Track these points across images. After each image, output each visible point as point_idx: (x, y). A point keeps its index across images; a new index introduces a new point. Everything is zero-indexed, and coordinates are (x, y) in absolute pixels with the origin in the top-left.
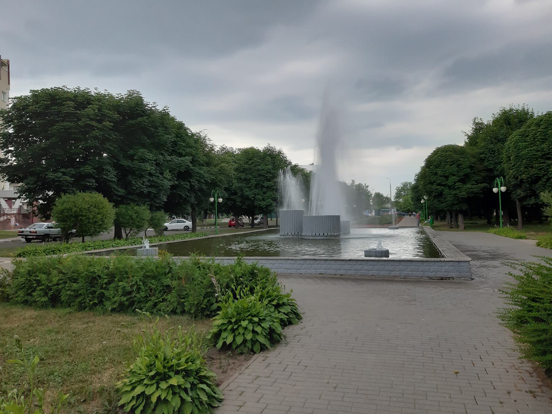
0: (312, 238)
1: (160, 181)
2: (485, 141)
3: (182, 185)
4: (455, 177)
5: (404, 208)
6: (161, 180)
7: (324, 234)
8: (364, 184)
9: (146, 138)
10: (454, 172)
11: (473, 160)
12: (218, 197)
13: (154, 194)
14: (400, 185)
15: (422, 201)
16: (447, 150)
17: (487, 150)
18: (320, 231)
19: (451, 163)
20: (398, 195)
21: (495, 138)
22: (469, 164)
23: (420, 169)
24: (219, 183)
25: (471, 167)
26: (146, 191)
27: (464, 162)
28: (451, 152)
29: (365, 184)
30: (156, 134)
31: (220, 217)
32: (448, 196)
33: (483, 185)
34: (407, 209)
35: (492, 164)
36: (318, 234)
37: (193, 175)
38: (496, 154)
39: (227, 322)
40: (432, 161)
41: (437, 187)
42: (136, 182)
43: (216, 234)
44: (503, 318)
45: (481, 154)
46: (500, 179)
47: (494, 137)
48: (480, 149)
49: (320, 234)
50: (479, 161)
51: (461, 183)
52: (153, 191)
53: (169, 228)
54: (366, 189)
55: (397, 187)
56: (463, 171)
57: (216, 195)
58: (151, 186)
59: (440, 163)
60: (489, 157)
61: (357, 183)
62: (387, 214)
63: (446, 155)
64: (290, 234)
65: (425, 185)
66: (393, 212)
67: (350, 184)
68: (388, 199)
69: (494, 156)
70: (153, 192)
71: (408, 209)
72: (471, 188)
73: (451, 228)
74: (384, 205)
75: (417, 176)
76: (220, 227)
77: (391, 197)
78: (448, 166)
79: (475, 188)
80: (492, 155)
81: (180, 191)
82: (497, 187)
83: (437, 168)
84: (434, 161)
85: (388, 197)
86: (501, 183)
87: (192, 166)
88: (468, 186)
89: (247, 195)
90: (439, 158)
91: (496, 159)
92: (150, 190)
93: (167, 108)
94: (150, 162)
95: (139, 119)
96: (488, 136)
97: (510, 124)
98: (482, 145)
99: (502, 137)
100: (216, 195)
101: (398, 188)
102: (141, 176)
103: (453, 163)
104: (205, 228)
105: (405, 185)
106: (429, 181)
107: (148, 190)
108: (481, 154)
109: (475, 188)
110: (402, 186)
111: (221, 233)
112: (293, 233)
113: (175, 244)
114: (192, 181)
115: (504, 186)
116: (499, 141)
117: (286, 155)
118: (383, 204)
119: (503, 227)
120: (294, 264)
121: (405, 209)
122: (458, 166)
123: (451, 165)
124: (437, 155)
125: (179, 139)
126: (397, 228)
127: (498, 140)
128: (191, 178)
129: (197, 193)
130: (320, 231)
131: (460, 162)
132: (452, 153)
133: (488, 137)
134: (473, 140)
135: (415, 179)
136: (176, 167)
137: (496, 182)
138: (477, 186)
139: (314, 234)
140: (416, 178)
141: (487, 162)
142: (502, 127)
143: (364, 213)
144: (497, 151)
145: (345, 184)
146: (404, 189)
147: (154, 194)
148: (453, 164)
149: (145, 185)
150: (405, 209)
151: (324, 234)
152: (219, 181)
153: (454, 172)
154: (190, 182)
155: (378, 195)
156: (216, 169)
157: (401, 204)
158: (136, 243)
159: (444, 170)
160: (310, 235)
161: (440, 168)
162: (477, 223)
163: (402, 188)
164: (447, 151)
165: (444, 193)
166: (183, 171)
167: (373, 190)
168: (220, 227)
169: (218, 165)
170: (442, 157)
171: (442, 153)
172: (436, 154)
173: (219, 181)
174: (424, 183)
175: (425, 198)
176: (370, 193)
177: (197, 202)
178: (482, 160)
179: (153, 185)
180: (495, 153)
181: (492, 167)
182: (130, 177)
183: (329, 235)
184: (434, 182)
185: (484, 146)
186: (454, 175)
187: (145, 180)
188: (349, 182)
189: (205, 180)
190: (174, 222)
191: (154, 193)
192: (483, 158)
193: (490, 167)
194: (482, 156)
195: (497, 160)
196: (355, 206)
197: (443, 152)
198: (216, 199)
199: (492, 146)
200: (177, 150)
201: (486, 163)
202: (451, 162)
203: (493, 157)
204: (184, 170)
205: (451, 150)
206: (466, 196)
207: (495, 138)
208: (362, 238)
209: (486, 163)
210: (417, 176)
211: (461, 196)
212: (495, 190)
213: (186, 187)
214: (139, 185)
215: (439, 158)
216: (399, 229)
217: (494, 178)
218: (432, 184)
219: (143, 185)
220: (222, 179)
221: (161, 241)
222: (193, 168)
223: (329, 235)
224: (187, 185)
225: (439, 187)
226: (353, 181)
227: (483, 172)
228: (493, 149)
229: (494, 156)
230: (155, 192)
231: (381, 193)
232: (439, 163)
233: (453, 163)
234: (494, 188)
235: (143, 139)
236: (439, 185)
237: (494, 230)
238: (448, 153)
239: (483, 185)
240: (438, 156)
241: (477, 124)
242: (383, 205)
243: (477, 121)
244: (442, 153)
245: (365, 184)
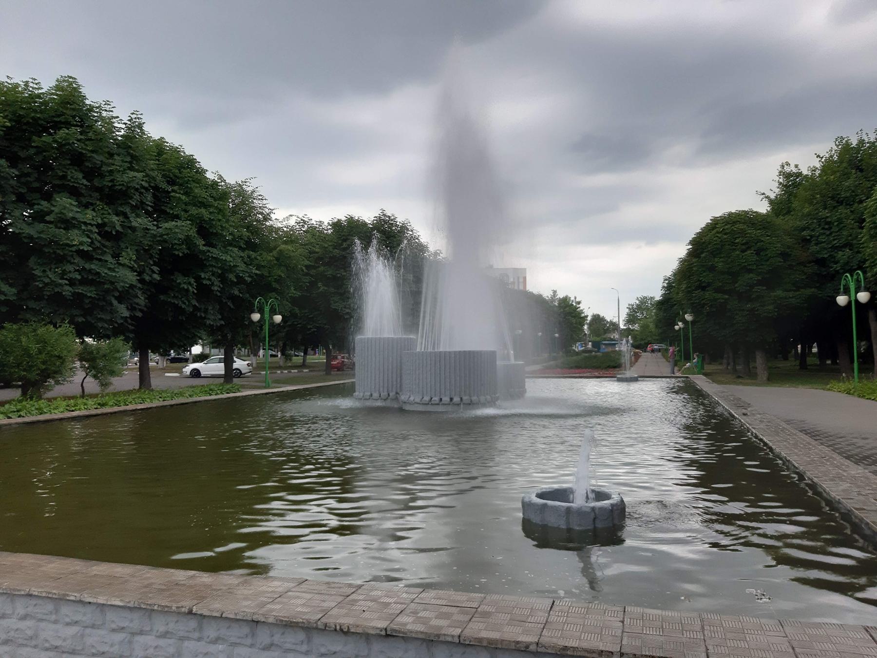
0: (421, 408)
1: (106, 271)
2: (811, 203)
3: (180, 284)
4: (751, 275)
5: (642, 339)
6: (109, 269)
7: (451, 399)
8: (572, 299)
9: (80, 175)
10: (750, 265)
11: (788, 240)
12: (273, 312)
13: (90, 300)
14: (635, 301)
15: (677, 327)
16: (735, 220)
17: (815, 221)
18: (443, 391)
19: (744, 247)
20: (631, 319)
21: (833, 198)
22: (782, 250)
23: (678, 262)
24: (275, 285)
25: (784, 255)
26: (67, 291)
27: (770, 244)
28: (744, 223)
29: (575, 298)
30: (104, 168)
31: (311, 352)
32: (737, 314)
33: (809, 291)
35: (825, 249)
36: (436, 399)
37: (206, 264)
38: (835, 229)
40: (704, 243)
41: (714, 295)
42: (44, 271)
43: (265, 388)
45: (804, 229)
46: (855, 277)
47: (830, 195)
48: (800, 221)
49: (441, 400)
50: (799, 244)
51: (765, 288)
52: (90, 292)
53: (203, 373)
54: (576, 306)
55: (629, 305)
56: (768, 263)
57: (267, 309)
58: (84, 282)
59: (722, 246)
60: (819, 236)
61: (561, 295)
62: (613, 350)
63: (732, 230)
64: (376, 395)
65: (689, 292)
66: (624, 347)
67: (550, 296)
68: (615, 326)
69: (831, 234)
70: (89, 295)
72: (786, 298)
73: (739, 377)
74: (608, 335)
75: (667, 282)
76: (310, 371)
77: (619, 321)
78: (738, 252)
79: (793, 297)
80: (825, 231)
81: (175, 297)
82: (847, 292)
83: (714, 257)
84: (709, 244)
85: (614, 321)
87: (204, 245)
88: (779, 293)
89: (335, 309)
90: (719, 235)
91: (834, 240)
92: (80, 290)
93: (139, 116)
94: (83, 228)
95: (63, 132)
96: (817, 194)
97: (861, 171)
98: (806, 211)
99: (848, 195)
100: (267, 309)
101: (631, 307)
102: (61, 260)
103: (747, 246)
104: (279, 372)
105: (643, 301)
106: (698, 283)
107: (72, 291)
108: (804, 229)
109: (793, 297)
110: (637, 302)
111: (279, 385)
112: (384, 394)
113: (175, 407)
114: (203, 277)
115: (866, 289)
116: (840, 203)
117: (418, 234)
118: (605, 333)
119: (860, 378)
120: (93, 626)
122: (758, 252)
123: (743, 251)
124: (715, 231)
125: (176, 188)
126: (635, 380)
127: (838, 202)
128: (203, 271)
129: (226, 303)
130: (443, 391)
131: (762, 243)
132: (745, 226)
133: (818, 196)
134: (781, 206)
135: (664, 287)
136: (153, 241)
137: (843, 282)
138: (798, 293)
139: (427, 398)
140: (666, 285)
141: (816, 244)
142: (846, 175)
143: (574, 348)
144: (836, 224)
145: (540, 297)
146: (641, 307)
147: (90, 300)
148: (749, 248)
149: (66, 279)
151: (451, 399)
152: (276, 281)
153: (750, 265)
154: (198, 279)
155: (597, 319)
156: (269, 257)
157: (637, 333)
158: (22, 413)
159: (730, 260)
160: (418, 400)
161: (721, 258)
162: (779, 368)
163: (637, 305)
164: (734, 222)
165: (728, 307)
166: (181, 255)
167: (589, 309)
168: (310, 371)
169: (275, 248)
170: (725, 234)
171: (726, 227)
172: (713, 230)
173: (276, 281)
174: (686, 288)
175: (688, 317)
176: (583, 313)
177: (224, 323)
178: (806, 241)
179: (90, 279)
180: (831, 228)
181: (826, 256)
182: (32, 262)
183: (464, 401)
184: (709, 285)
185: (809, 214)
186: (750, 271)
187: (69, 268)
188: (547, 294)
189: (237, 277)
190: (211, 361)
191: (91, 297)
192: (809, 238)
193: (821, 256)
194: (804, 233)
195: (835, 242)
196: (557, 335)
197: (726, 225)
198: (267, 316)
199: (825, 213)
200: (168, 210)
201: (814, 248)
202: (743, 244)
203: (827, 235)
204: (183, 253)
205: (743, 221)
206: (776, 314)
207: (833, 198)
209: (814, 248)
210: (667, 282)
211: (766, 314)
212: (842, 300)
213: (186, 287)
214: (50, 278)
215: (719, 235)
216: (639, 383)
217: (835, 277)
218: (704, 288)
219: (62, 278)
220: (280, 276)
221: (102, 405)
222: (205, 248)
223: (464, 401)
224: (190, 283)
225: (720, 295)
226: (555, 292)
227: (808, 265)
228: (829, 220)
229: (831, 234)
230: (93, 296)
231: (602, 315)
232: (719, 246)
233: (747, 246)
234: (838, 294)
235: (72, 177)
236: (717, 290)
237: (842, 386)
238: (741, 226)
239: (809, 291)
240: (718, 232)
241: (787, 176)
242: (607, 334)
243: (787, 169)
244: (726, 227)
245: (575, 298)
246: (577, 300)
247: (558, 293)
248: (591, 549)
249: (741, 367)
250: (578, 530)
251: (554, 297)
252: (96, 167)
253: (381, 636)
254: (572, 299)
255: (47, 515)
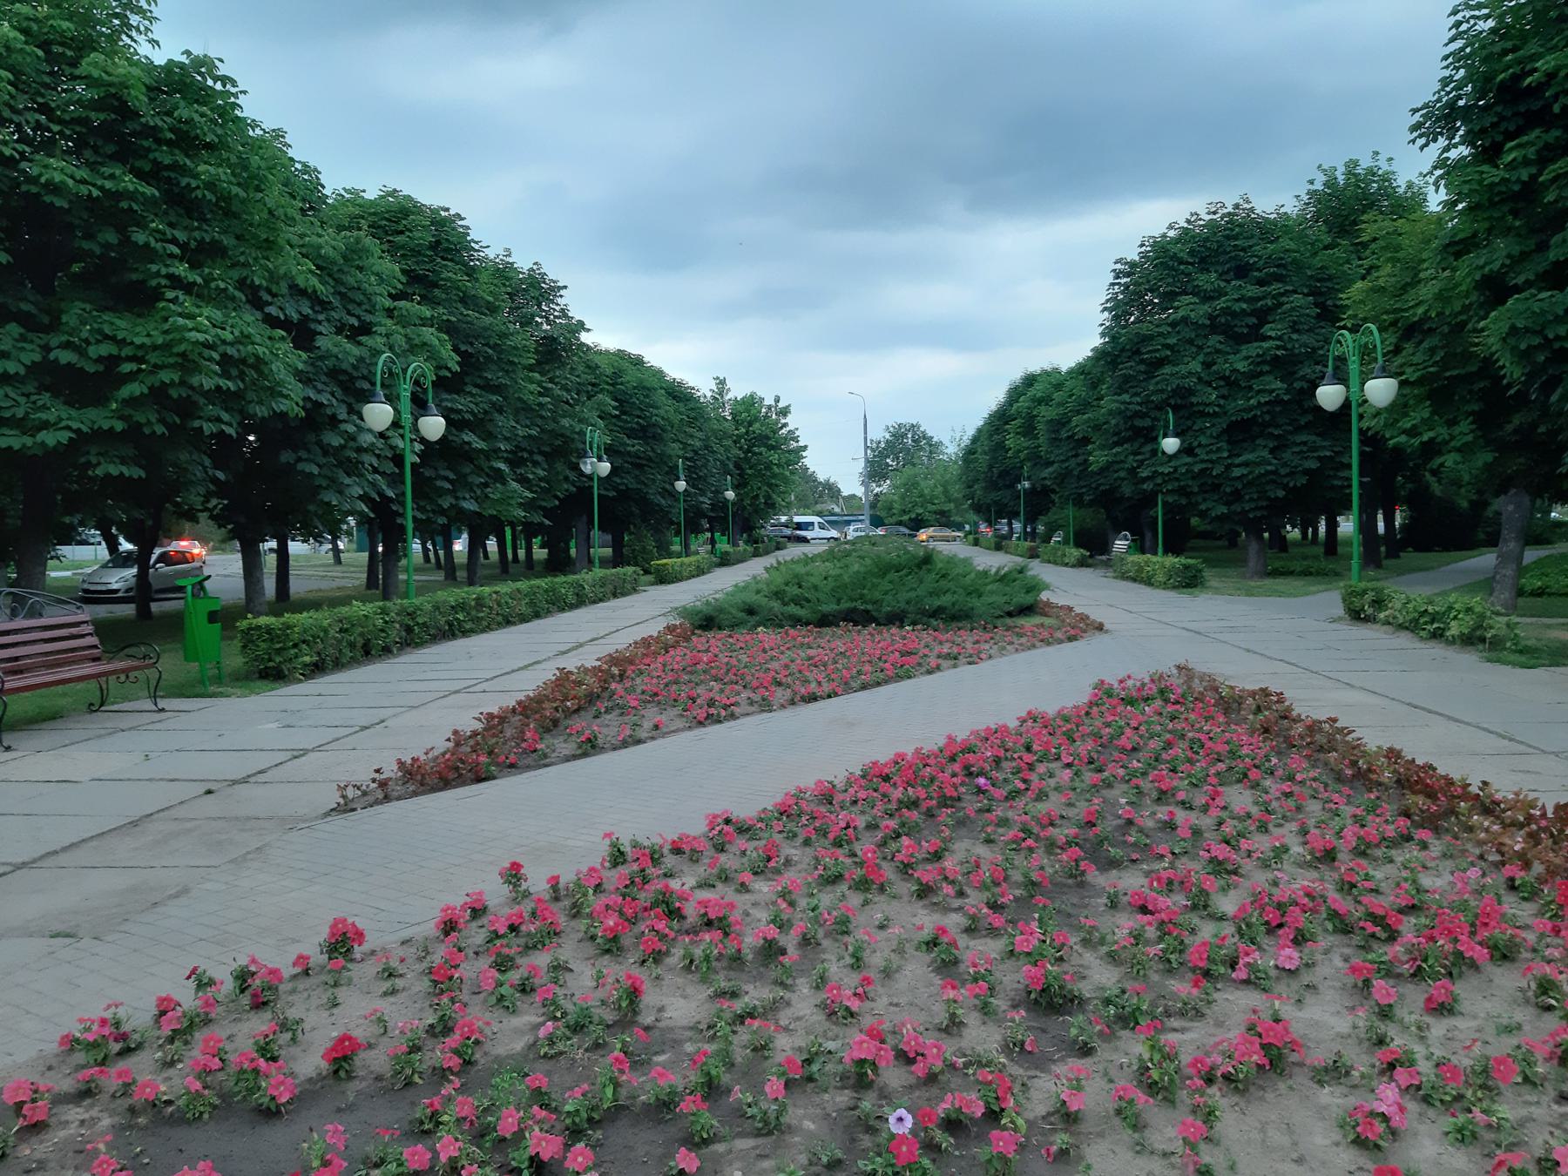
5: (904, 512)
8: (769, 401)
29: (777, 400)
34: (913, 516)
39: (1533, 247)
44: (949, 737)
57: (406, 390)
67: (709, 394)
71: (918, 515)
82: (1341, 378)
86: (1366, 353)
110: (888, 436)
121: (906, 518)
150: (906, 518)
208: (1457, 721)
226: (721, 383)
245: (777, 400)
246: (781, 405)
247: (729, 384)
248: (233, 551)
249: (53, 574)
250: (179, 538)
251: (721, 394)
252: (115, 336)
253: (928, 859)
254: (766, 403)
255: (1450, 225)
